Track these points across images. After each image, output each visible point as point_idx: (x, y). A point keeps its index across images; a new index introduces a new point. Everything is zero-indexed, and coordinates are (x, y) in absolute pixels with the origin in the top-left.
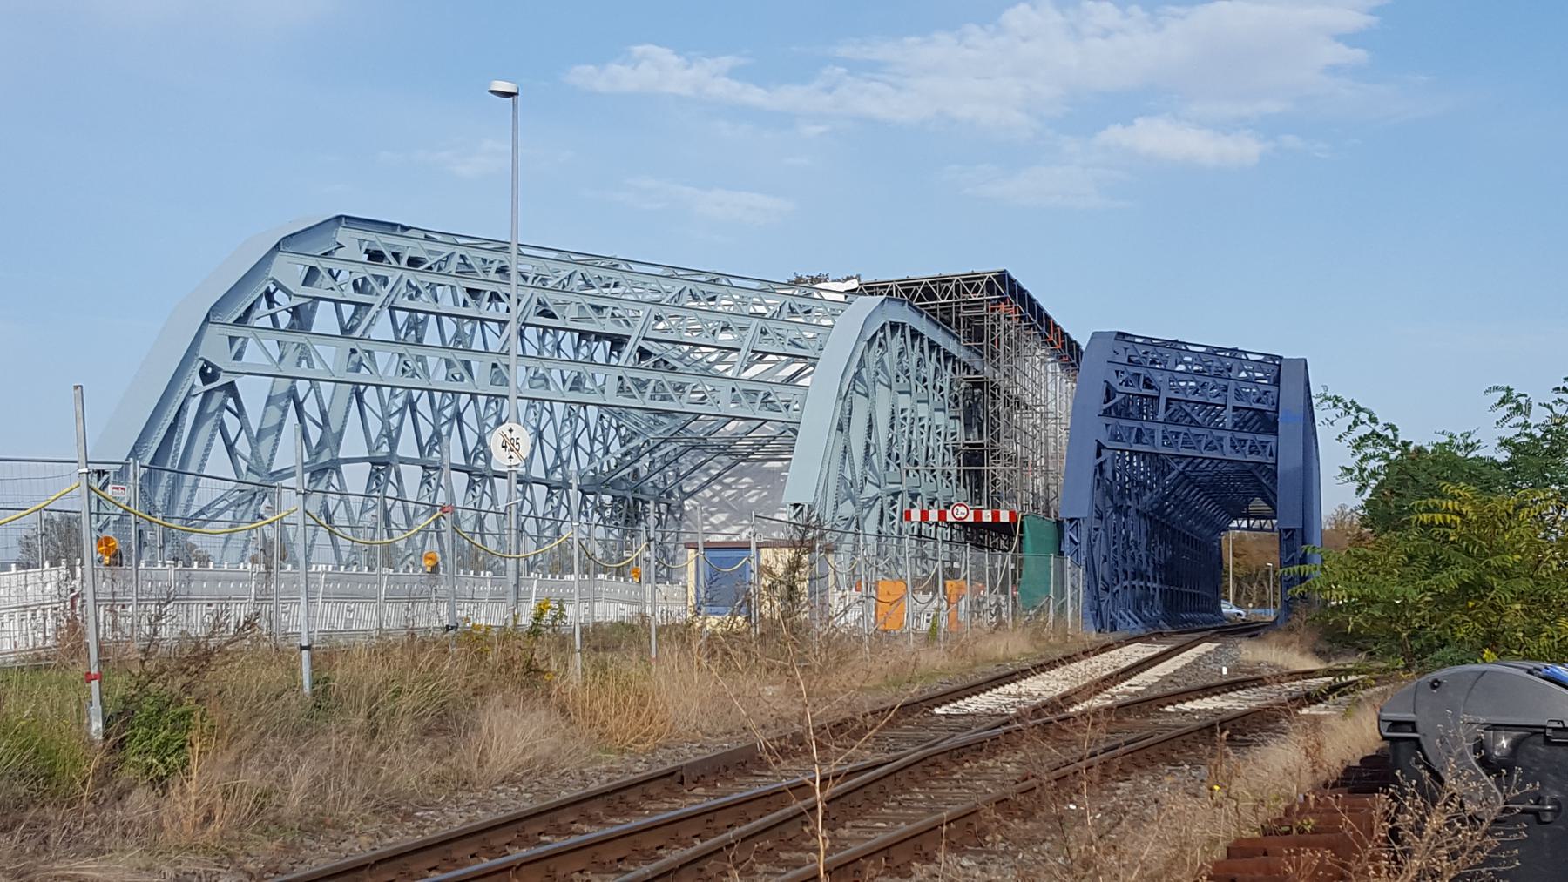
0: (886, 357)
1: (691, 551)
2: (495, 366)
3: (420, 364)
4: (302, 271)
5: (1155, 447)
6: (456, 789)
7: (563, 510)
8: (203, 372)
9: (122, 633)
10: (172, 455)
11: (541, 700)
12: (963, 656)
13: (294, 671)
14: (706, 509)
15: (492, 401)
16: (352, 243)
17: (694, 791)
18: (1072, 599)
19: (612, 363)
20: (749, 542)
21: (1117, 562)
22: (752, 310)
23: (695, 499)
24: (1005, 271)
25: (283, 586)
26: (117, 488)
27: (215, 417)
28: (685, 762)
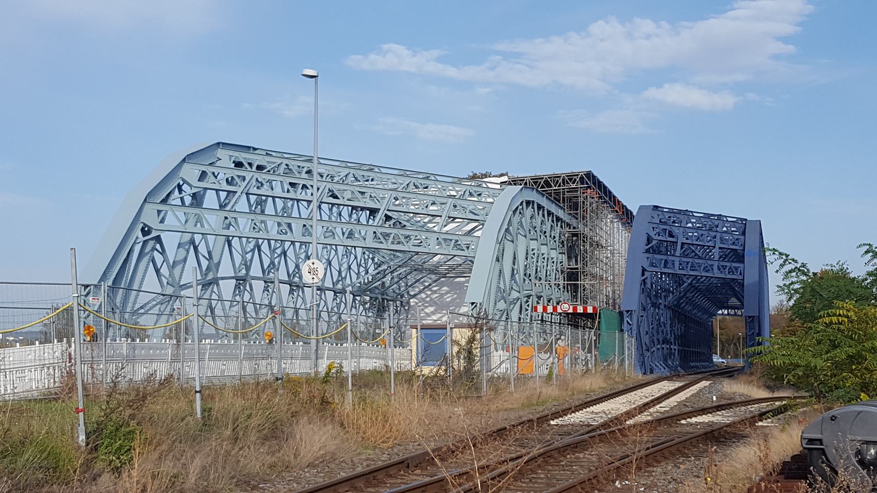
0: (523, 220)
1: (414, 330)
2: (304, 226)
3: (263, 224)
4: (198, 174)
5: (675, 271)
6: (282, 471)
7: (343, 305)
8: (143, 230)
9: (97, 379)
10: (125, 275)
11: (329, 419)
12: (567, 389)
13: (192, 402)
14: (423, 304)
15: (303, 245)
16: (225, 158)
17: (415, 472)
18: (628, 355)
19: (370, 224)
20: (446, 325)
21: (653, 335)
22: (448, 193)
23: (417, 299)
24: (590, 171)
25: (186, 352)
26: (95, 299)
27: (149, 255)
28: (410, 455)
